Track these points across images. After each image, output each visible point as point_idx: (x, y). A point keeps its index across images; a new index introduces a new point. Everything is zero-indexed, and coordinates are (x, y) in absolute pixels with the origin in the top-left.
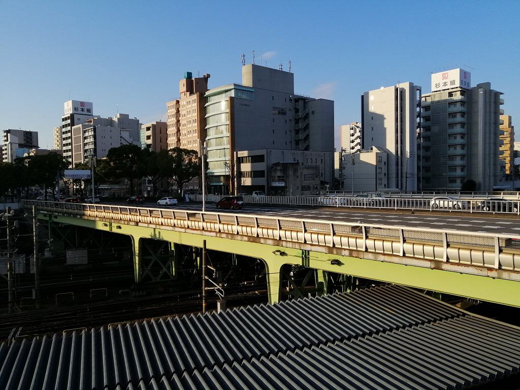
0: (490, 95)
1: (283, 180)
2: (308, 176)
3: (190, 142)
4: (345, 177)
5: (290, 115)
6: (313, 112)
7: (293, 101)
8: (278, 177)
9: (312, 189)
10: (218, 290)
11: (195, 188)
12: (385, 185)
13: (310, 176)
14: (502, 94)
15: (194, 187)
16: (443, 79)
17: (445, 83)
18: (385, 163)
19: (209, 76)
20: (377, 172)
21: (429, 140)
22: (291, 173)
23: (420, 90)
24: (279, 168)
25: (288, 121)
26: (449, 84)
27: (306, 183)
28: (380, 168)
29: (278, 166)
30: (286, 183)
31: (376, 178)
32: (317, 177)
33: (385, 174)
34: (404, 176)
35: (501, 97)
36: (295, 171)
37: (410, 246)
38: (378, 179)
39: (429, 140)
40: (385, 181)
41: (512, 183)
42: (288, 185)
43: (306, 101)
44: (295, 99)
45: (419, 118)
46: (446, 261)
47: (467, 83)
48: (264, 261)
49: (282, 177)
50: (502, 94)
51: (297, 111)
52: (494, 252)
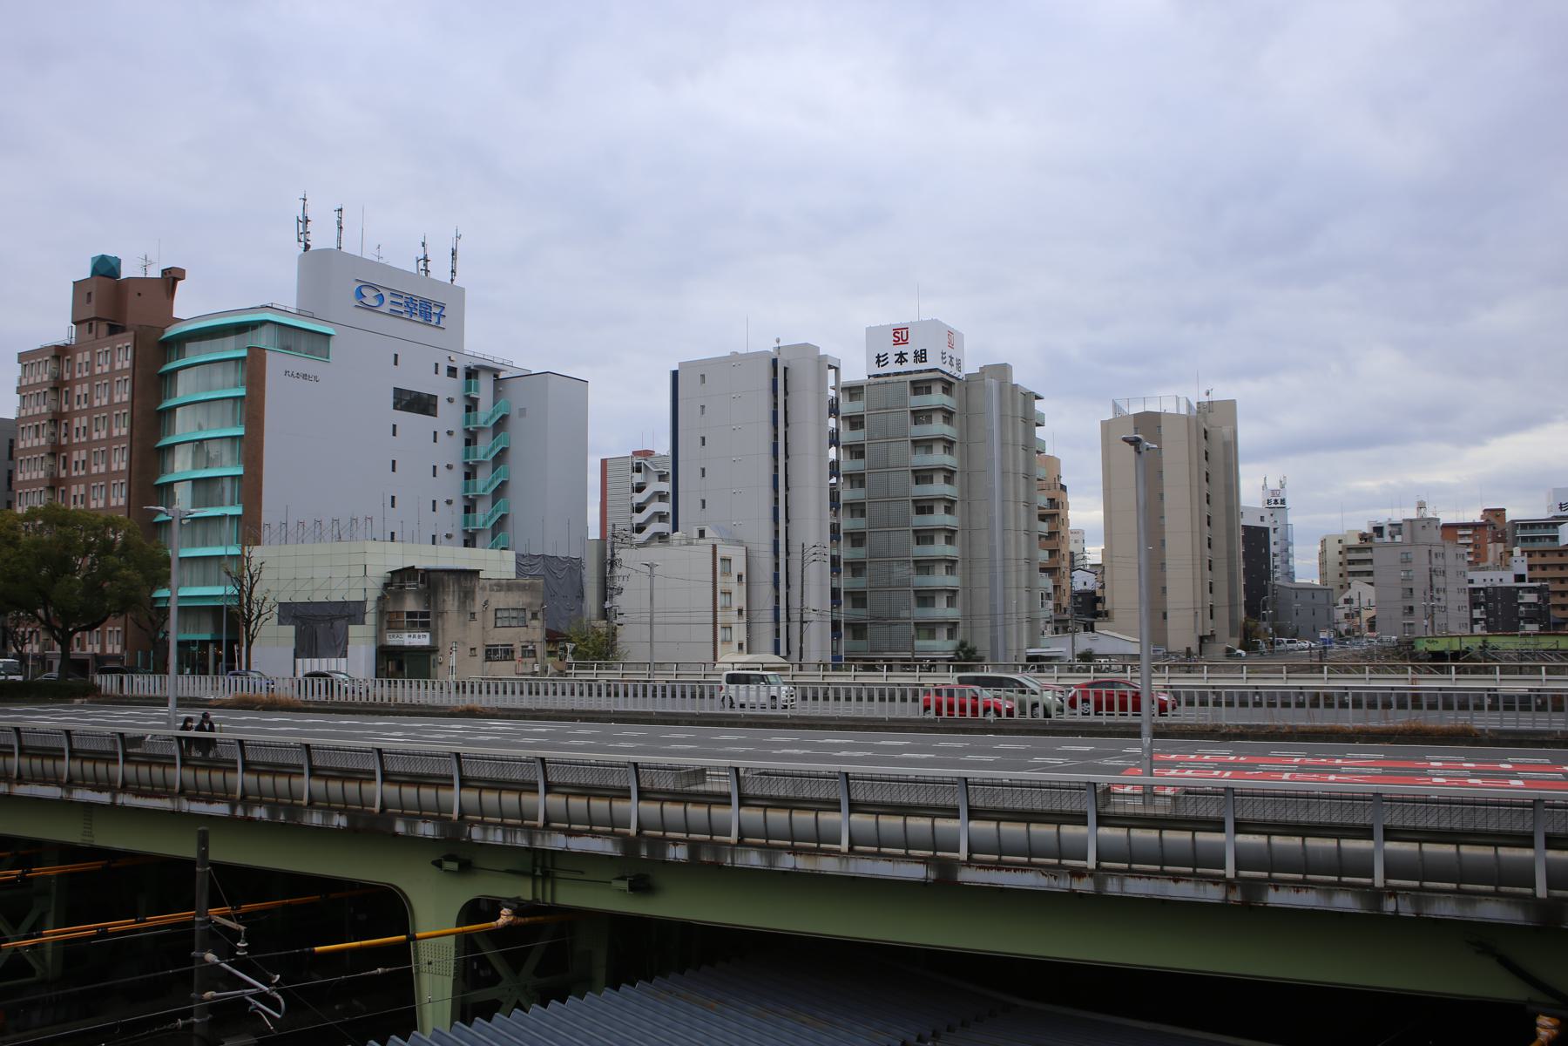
0: (1014, 400)
1: (425, 626)
2: (506, 614)
3: (1329, 658)
4: (620, 619)
5: (450, 416)
6: (522, 412)
7: (461, 374)
8: (410, 615)
9: (518, 655)
10: (262, 997)
11: (109, 650)
12: (740, 646)
13: (514, 614)
14: (1038, 398)
15: (103, 648)
16: (896, 343)
17: (901, 355)
18: (740, 577)
19: (1125, 440)
20: (719, 605)
21: (863, 514)
22: (451, 603)
23: (837, 369)
24: (410, 586)
25: (442, 436)
26: (910, 357)
27: (500, 637)
28: (724, 593)
29: (409, 579)
30: (434, 636)
31: (715, 624)
32: (534, 616)
33: (740, 611)
34: (795, 616)
35: (1038, 405)
36: (467, 596)
37: (561, 800)
38: (719, 626)
39: (863, 514)
40: (739, 634)
41: (1070, 638)
42: (440, 645)
43: (502, 376)
44: (468, 368)
45: (834, 448)
46: (847, 850)
47: (954, 362)
48: (392, 885)
49: (424, 615)
50: (1038, 398)
51: (471, 406)
52: (730, 804)
